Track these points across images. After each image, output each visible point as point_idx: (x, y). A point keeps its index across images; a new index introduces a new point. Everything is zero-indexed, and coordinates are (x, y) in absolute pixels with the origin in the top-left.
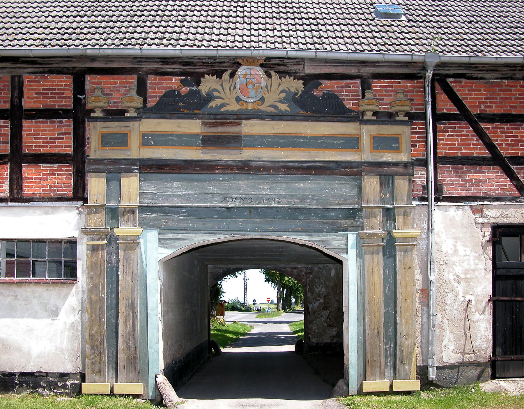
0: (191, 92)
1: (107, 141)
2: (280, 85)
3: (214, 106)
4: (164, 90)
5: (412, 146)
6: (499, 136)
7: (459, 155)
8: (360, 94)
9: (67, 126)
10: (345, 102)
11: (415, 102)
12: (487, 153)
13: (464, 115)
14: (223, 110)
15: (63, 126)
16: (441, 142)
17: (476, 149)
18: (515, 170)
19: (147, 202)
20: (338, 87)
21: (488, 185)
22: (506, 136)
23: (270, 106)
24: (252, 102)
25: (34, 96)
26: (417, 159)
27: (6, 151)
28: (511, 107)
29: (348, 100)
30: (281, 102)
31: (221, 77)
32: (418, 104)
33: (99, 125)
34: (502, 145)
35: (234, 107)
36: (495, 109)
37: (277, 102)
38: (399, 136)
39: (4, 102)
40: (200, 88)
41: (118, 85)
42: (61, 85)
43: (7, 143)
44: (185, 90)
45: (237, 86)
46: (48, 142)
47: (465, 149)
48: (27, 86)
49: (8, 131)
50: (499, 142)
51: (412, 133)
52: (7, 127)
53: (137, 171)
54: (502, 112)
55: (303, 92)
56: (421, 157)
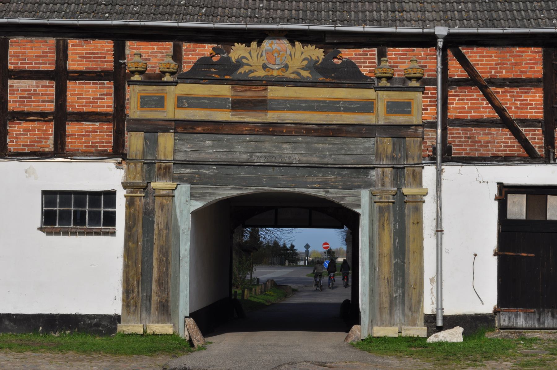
0: (222, 58)
1: (145, 102)
2: (302, 53)
3: (243, 72)
4: (197, 57)
5: (424, 110)
6: (509, 100)
7: (469, 118)
8: (376, 61)
9: (108, 88)
10: (362, 69)
11: (428, 68)
12: (496, 116)
13: (473, 80)
14: (251, 75)
15: (105, 88)
16: (452, 106)
17: (486, 112)
18: (524, 132)
19: (180, 157)
20: (356, 55)
21: (495, 146)
22: (515, 100)
23: (293, 73)
24: (277, 69)
25: (78, 59)
26: (428, 122)
27: (51, 109)
28: (521, 72)
29: (364, 67)
30: (303, 69)
31: (249, 46)
32: (431, 71)
33: (138, 88)
34: (511, 108)
35: (261, 73)
36: (504, 74)
37: (300, 69)
38: (411, 101)
39: (49, 64)
40: (230, 55)
41: (156, 50)
42: (103, 50)
43: (52, 102)
44: (216, 59)
45: (264, 54)
46: (90, 102)
47: (475, 112)
48: (72, 50)
49: (53, 91)
50: (508, 105)
51: (424, 98)
52: (52, 87)
53: (172, 131)
54: (513, 77)
55: (324, 60)
56: (432, 120)
